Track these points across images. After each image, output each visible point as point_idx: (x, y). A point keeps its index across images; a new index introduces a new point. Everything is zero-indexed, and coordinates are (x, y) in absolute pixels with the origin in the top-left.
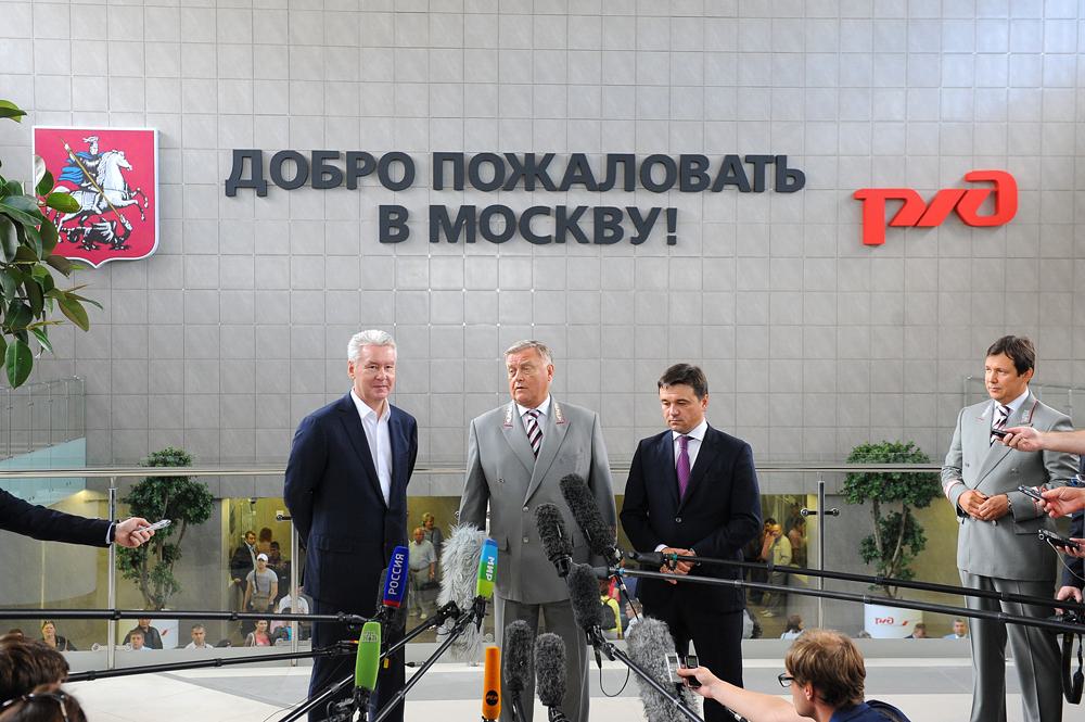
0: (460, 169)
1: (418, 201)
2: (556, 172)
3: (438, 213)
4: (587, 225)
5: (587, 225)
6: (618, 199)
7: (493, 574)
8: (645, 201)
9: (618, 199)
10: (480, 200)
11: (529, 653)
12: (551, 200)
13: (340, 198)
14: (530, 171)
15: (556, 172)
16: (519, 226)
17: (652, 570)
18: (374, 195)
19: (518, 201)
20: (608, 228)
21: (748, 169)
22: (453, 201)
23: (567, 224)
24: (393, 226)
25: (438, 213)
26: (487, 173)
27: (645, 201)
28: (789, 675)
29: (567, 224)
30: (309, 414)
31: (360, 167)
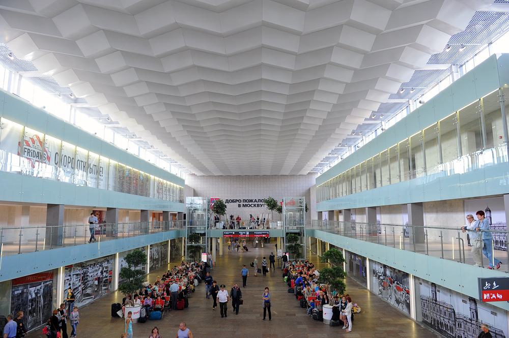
0: (246, 201)
1: (241, 204)
2: (254, 201)
3: (243, 205)
4: (256, 205)
5: (256, 205)
6: (259, 203)
7: (71, 186)
8: (261, 203)
9: (259, 203)
10: (247, 203)
11: (92, 163)
12: (257, 203)
13: (235, 203)
14: (251, 201)
15: (254, 201)
16: (250, 206)
17: (398, 125)
18: (238, 203)
19: (250, 203)
20: (258, 206)
21: (361, 220)
22: (245, 204)
23: (255, 205)
24: (239, 206)
25: (243, 205)
26: (248, 201)
27: (261, 203)
28: (359, 177)
29: (255, 205)
30: (51, 113)
31: (237, 201)
